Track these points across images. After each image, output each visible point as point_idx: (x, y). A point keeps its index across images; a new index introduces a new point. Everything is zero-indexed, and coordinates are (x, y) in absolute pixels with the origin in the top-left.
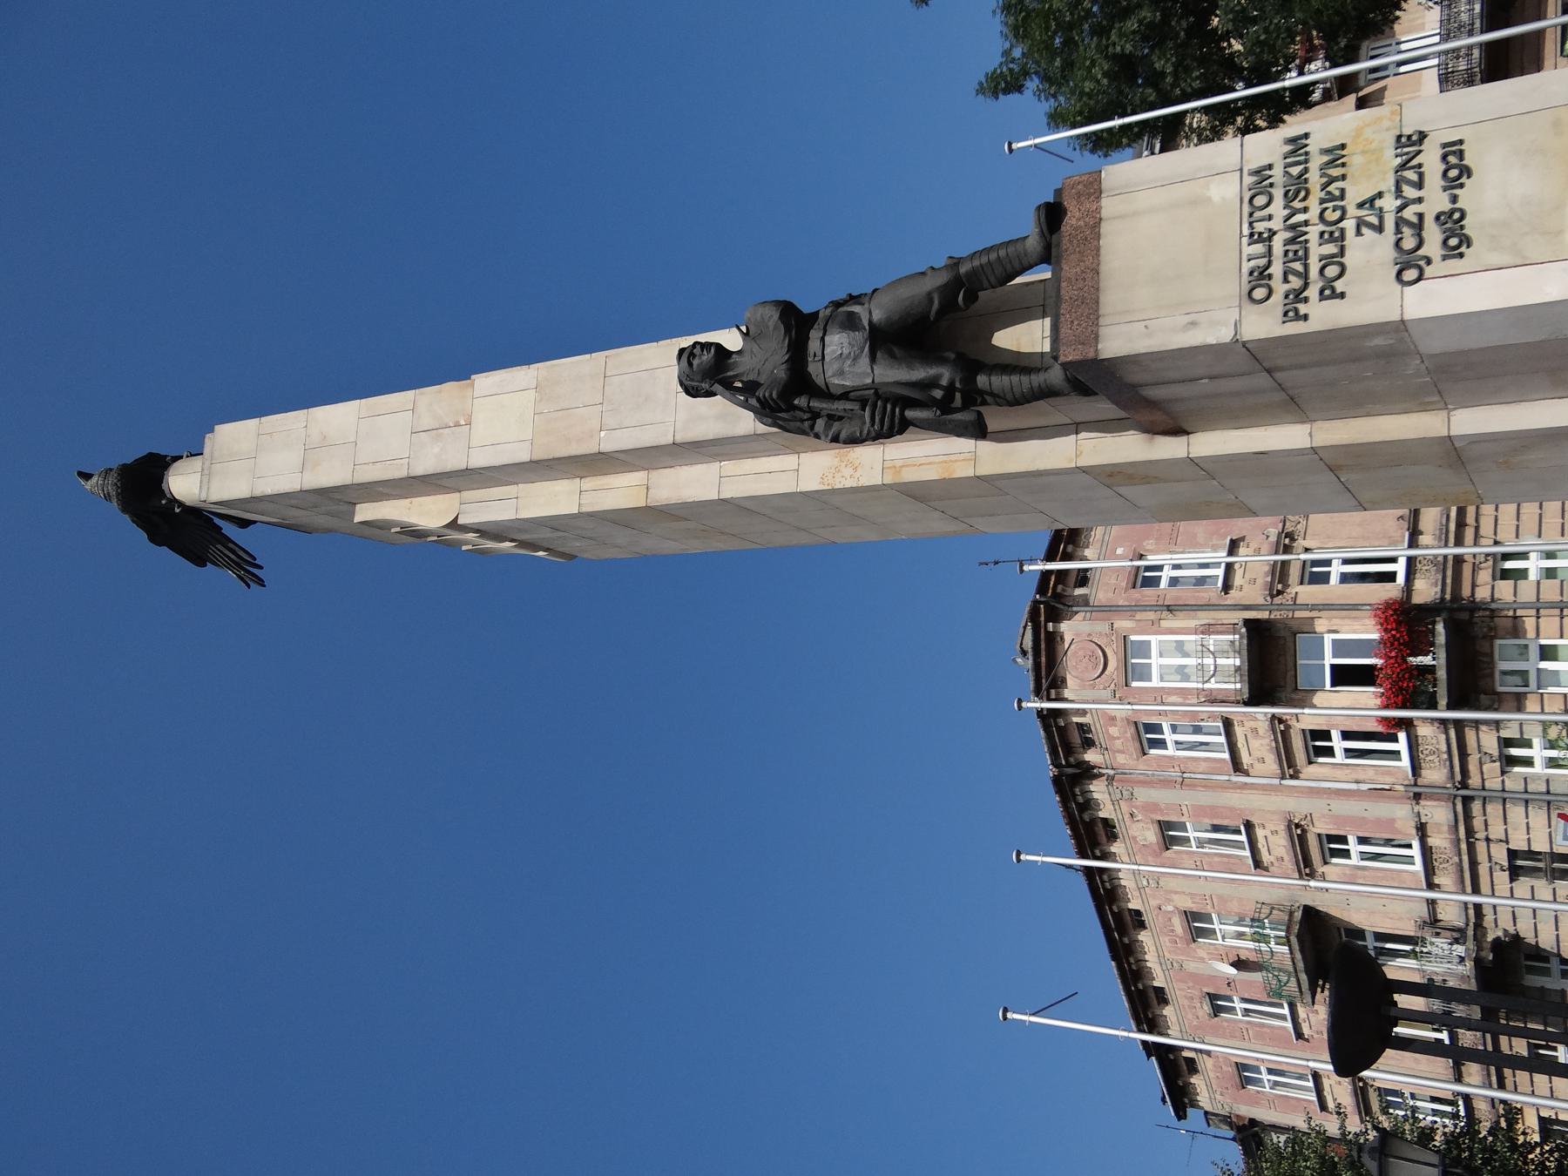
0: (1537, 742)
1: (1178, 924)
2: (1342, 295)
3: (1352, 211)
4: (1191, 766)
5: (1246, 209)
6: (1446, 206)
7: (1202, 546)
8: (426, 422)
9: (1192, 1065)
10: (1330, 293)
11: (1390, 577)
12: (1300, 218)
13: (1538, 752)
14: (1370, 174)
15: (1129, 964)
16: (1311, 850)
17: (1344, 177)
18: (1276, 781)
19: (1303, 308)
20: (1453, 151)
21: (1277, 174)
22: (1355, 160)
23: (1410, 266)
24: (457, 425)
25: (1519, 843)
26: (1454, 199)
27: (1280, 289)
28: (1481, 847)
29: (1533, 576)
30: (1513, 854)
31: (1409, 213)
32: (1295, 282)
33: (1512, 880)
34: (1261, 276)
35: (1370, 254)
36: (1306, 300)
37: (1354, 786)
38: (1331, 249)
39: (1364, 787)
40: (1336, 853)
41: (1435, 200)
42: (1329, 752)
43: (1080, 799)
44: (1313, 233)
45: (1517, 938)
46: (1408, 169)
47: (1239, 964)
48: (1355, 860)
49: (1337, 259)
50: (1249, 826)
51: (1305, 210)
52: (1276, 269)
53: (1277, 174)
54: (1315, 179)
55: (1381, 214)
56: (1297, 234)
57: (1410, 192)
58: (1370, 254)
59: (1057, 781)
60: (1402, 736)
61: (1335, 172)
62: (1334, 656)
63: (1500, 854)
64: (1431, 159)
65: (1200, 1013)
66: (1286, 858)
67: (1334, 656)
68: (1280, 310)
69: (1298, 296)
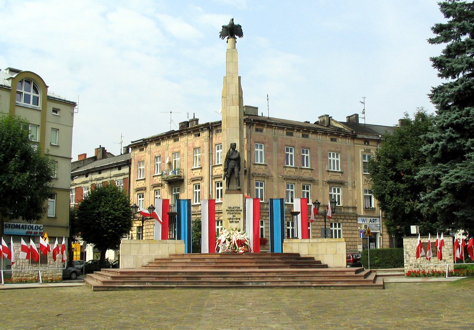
1: (176, 150)
7: (266, 157)
14: (237, 216)
16: (197, 181)
20: (238, 222)
29: (331, 229)
34: (230, 208)
40: (196, 186)
42: (218, 186)
47: (170, 164)
48: (195, 191)
50: (201, 168)
58: (231, 216)
59: (208, 124)
64: (238, 220)
65: (156, 154)
69: (228, 211)
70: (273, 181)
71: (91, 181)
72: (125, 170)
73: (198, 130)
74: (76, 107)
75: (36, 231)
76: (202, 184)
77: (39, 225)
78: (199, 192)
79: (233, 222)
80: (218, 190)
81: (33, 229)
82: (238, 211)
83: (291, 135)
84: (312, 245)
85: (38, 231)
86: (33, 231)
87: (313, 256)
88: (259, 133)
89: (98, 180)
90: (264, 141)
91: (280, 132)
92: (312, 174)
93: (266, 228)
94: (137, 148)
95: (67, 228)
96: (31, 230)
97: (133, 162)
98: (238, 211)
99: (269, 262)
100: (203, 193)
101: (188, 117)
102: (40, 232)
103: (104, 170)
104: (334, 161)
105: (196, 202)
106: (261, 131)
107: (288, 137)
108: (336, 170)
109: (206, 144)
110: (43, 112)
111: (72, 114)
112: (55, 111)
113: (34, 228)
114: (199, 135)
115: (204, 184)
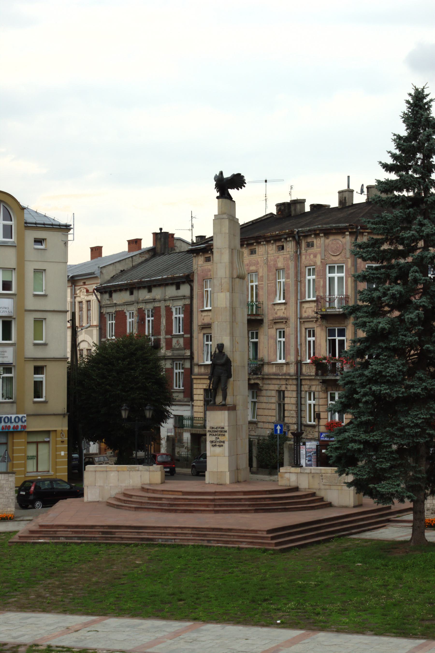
0: (314, 402)
4: (303, 284)
8: (223, 281)
10: (210, 435)
13: (312, 402)
18: (299, 317)
20: (222, 446)
21: (223, 430)
22: (223, 437)
23: (212, 442)
25: (286, 394)
27: (211, 430)
28: (284, 382)
30: (284, 391)
33: (277, 390)
34: (213, 428)
35: (213, 438)
37: (299, 343)
39: (299, 347)
41: (217, 444)
44: (216, 433)
45: (261, 390)
46: (221, 442)
49: (213, 435)
52: (213, 430)
54: (222, 433)
56: (217, 431)
58: (213, 438)
62: (339, 340)
63: (283, 388)
64: (222, 444)
66: (277, 316)
67: (339, 340)
69: (210, 431)
71: (138, 303)
72: (185, 290)
73: (280, 240)
74: (71, 231)
75: (15, 424)
76: (287, 331)
77: (20, 416)
79: (215, 445)
81: (11, 422)
82: (222, 432)
84: (313, 477)
85: (20, 424)
86: (12, 426)
87: (314, 491)
89: (146, 302)
95: (64, 415)
96: (9, 424)
97: (196, 278)
98: (222, 432)
99: (231, 505)
100: (289, 345)
101: (290, 194)
102: (22, 426)
103: (155, 286)
109: (292, 264)
110: (19, 248)
111: (66, 244)
112: (39, 241)
113: (13, 420)
114: (283, 248)
115: (290, 330)
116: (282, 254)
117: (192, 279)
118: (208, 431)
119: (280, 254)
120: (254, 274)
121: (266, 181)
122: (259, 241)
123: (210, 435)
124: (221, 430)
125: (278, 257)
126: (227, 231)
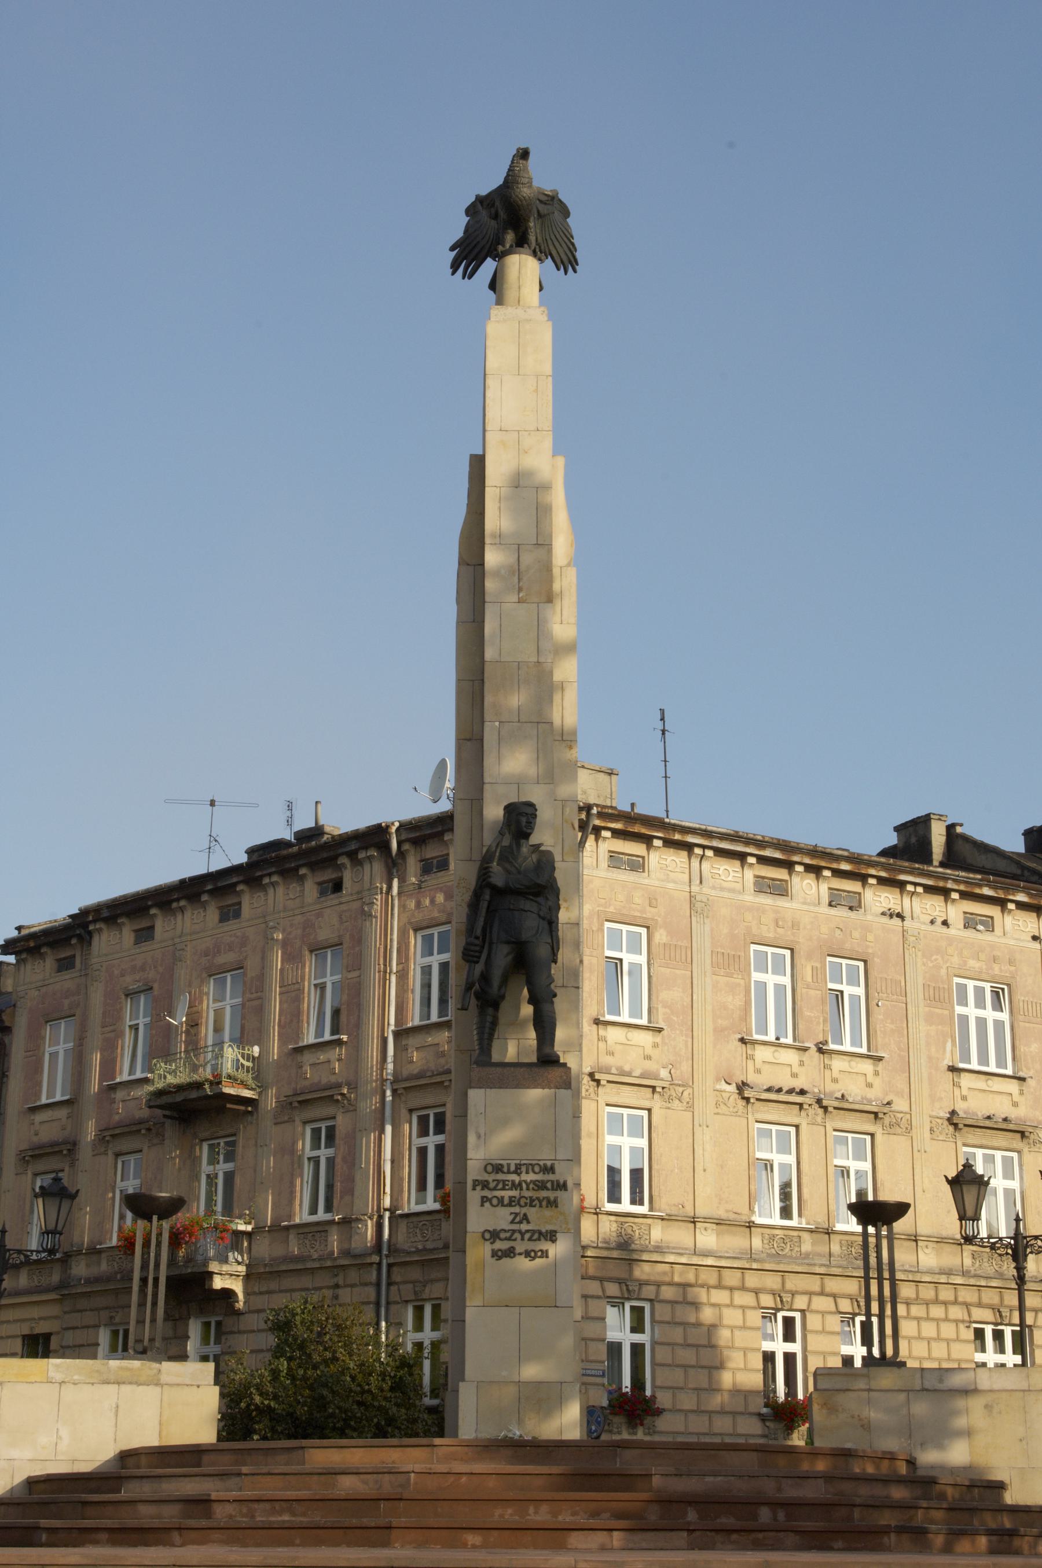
0: (436, 1335)
1: (226, 958)
2: (482, 1205)
3: (524, 1210)
5: (534, 1162)
6: (518, 1250)
9: (65, 965)
10: (484, 1200)
11: (614, 1196)
12: (524, 1186)
15: (178, 900)
17: (541, 1206)
19: (479, 1188)
21: (551, 1177)
22: (548, 1213)
23: (494, 1235)
24: (520, 590)
26: (520, 1254)
27: (490, 1178)
31: (517, 1235)
32: (492, 1185)
34: (498, 1169)
35: (501, 1218)
36: (482, 1189)
38: (506, 1201)
40: (316, 1132)
43: (362, 855)
51: (528, 1189)
52: (500, 1176)
53: (551, 1177)
54: (544, 1194)
55: (520, 1222)
56: (515, 1186)
57: (527, 1236)
58: (501, 1218)
60: (437, 1206)
61: (544, 1203)
65: (128, 979)
68: (479, 1178)
69: (485, 1185)
70: (690, 1107)
73: (331, 862)
78: (440, 1149)
79: (510, 1253)
80: (423, 1152)
83: (780, 890)
88: (624, 876)
90: (650, 912)
91: (726, 871)
92: (877, 1082)
93: (654, 1343)
94: (42, 956)
98: (541, 1186)
104: (981, 1022)
105: (313, 1211)
106: (637, 865)
107: (766, 900)
108: (992, 1068)
116: (336, 902)
117: (7, 1024)
118: (476, 1183)
119: (329, 903)
120: (228, 975)
121: (212, 803)
122: (258, 874)
123: (484, 1200)
124: (539, 1177)
125: (319, 915)
126: (548, 368)
